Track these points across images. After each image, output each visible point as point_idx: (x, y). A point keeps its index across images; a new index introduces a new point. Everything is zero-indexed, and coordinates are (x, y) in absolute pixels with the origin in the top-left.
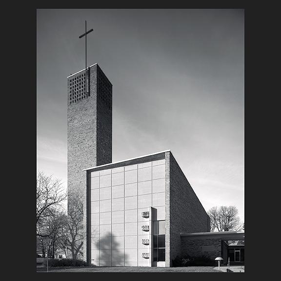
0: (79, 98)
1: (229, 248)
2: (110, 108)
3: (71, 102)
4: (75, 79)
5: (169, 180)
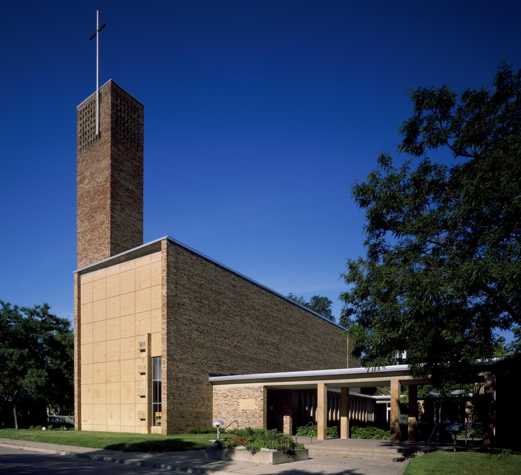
5: (165, 287)
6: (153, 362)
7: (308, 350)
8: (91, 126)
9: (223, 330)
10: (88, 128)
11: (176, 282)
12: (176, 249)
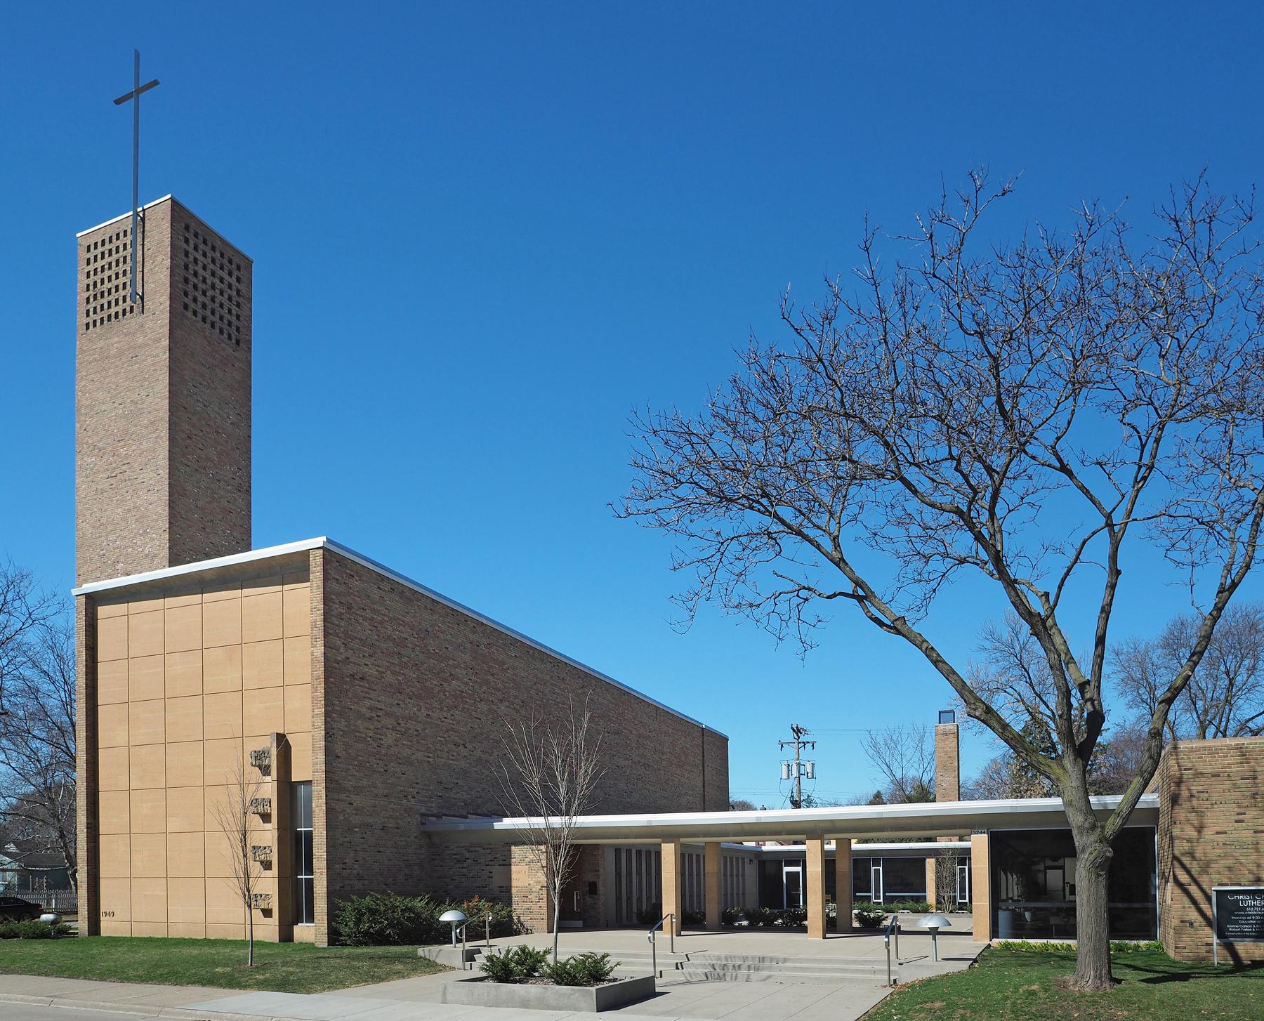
0: (113, 311)
1: (765, 858)
2: (241, 339)
3: (88, 325)
4: (103, 244)
5: (320, 643)
6: (289, 790)
7: (626, 763)
8: (110, 273)
9: (453, 730)
10: (107, 285)
11: (345, 632)
12: (992, 536)
